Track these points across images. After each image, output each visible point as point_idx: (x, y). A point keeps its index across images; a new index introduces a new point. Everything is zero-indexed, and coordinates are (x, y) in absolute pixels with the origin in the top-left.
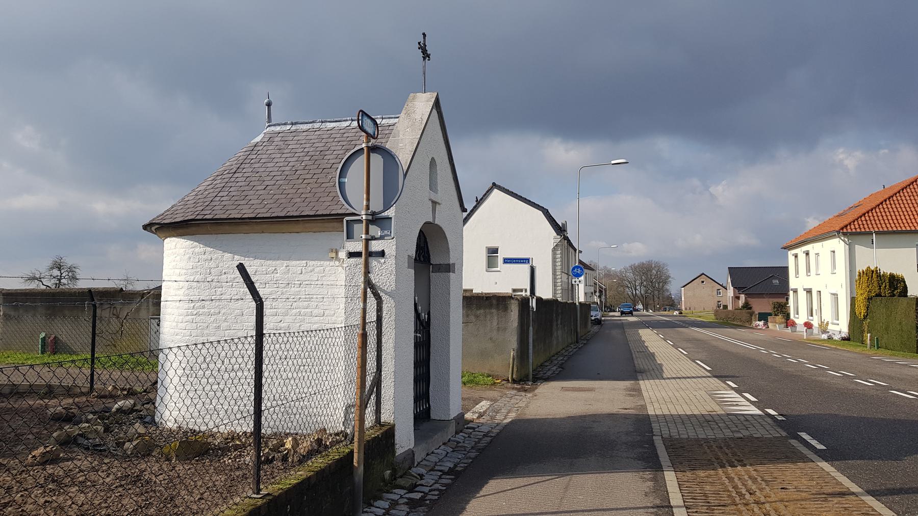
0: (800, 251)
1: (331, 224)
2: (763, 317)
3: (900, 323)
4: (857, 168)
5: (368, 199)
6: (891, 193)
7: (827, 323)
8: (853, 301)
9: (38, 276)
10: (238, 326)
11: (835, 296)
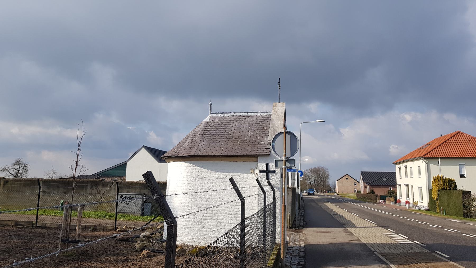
0: (402, 166)
1: (252, 159)
2: (383, 198)
3: (455, 203)
4: (431, 125)
5: (285, 152)
6: (446, 139)
7: (418, 202)
8: (430, 192)
9: (7, 169)
10: (210, 200)
11: (421, 189)
